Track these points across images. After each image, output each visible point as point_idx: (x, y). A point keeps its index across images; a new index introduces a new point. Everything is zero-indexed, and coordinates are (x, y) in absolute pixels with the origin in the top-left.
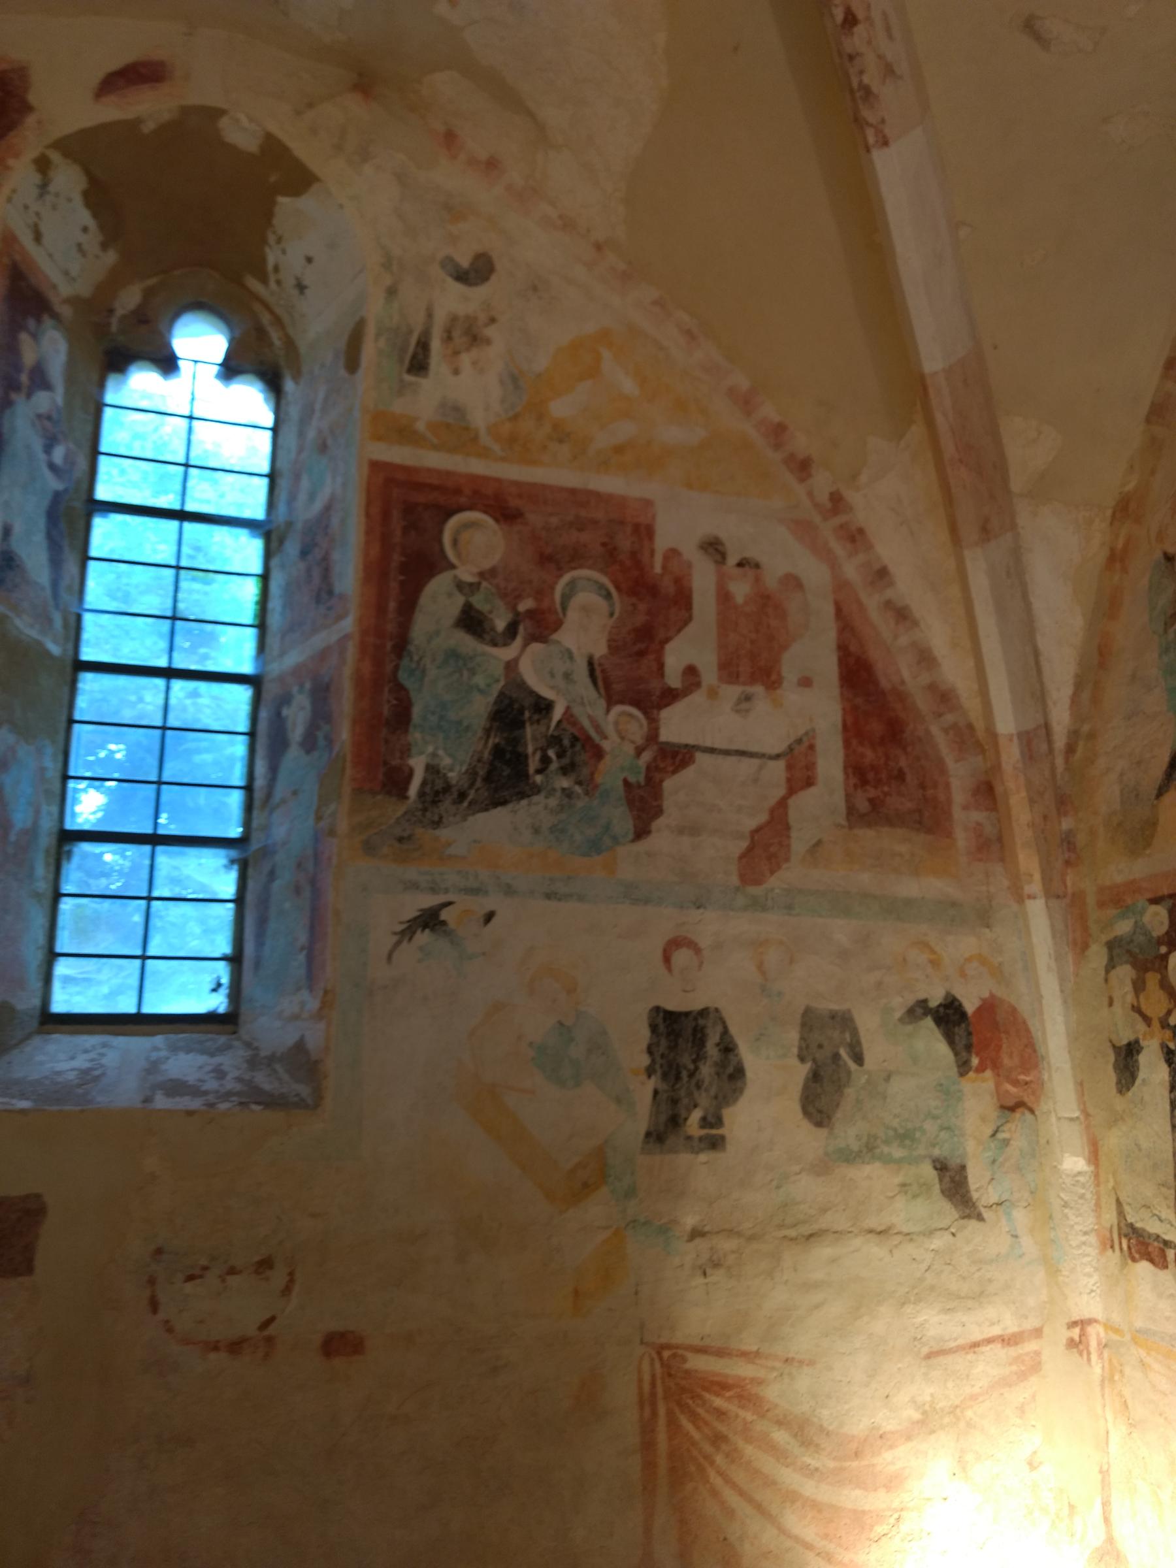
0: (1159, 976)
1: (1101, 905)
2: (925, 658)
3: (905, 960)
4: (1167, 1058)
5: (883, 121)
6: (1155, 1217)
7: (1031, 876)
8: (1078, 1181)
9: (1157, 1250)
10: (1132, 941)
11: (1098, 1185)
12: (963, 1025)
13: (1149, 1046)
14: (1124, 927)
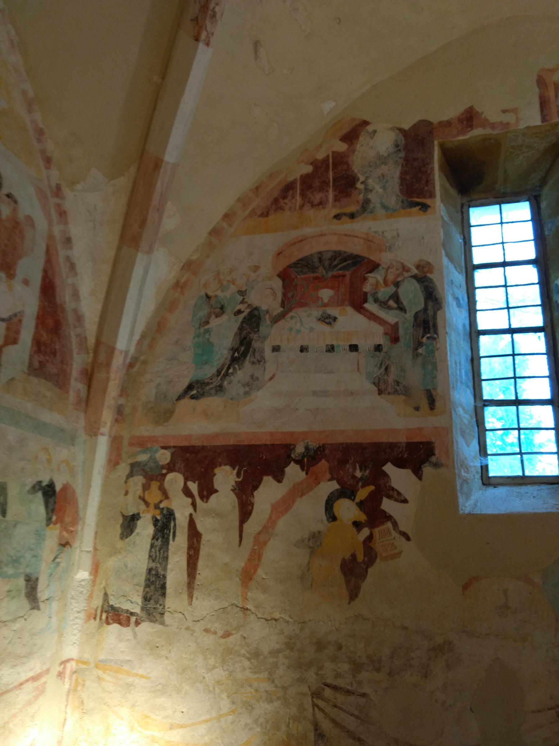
0: (159, 484)
1: (131, 444)
2: (76, 295)
3: (37, 457)
4: (155, 523)
5: (212, 34)
6: (129, 601)
7: (106, 423)
8: (81, 584)
9: (125, 617)
10: (146, 465)
11: (94, 586)
12: (53, 497)
13: (145, 517)
14: (143, 458)
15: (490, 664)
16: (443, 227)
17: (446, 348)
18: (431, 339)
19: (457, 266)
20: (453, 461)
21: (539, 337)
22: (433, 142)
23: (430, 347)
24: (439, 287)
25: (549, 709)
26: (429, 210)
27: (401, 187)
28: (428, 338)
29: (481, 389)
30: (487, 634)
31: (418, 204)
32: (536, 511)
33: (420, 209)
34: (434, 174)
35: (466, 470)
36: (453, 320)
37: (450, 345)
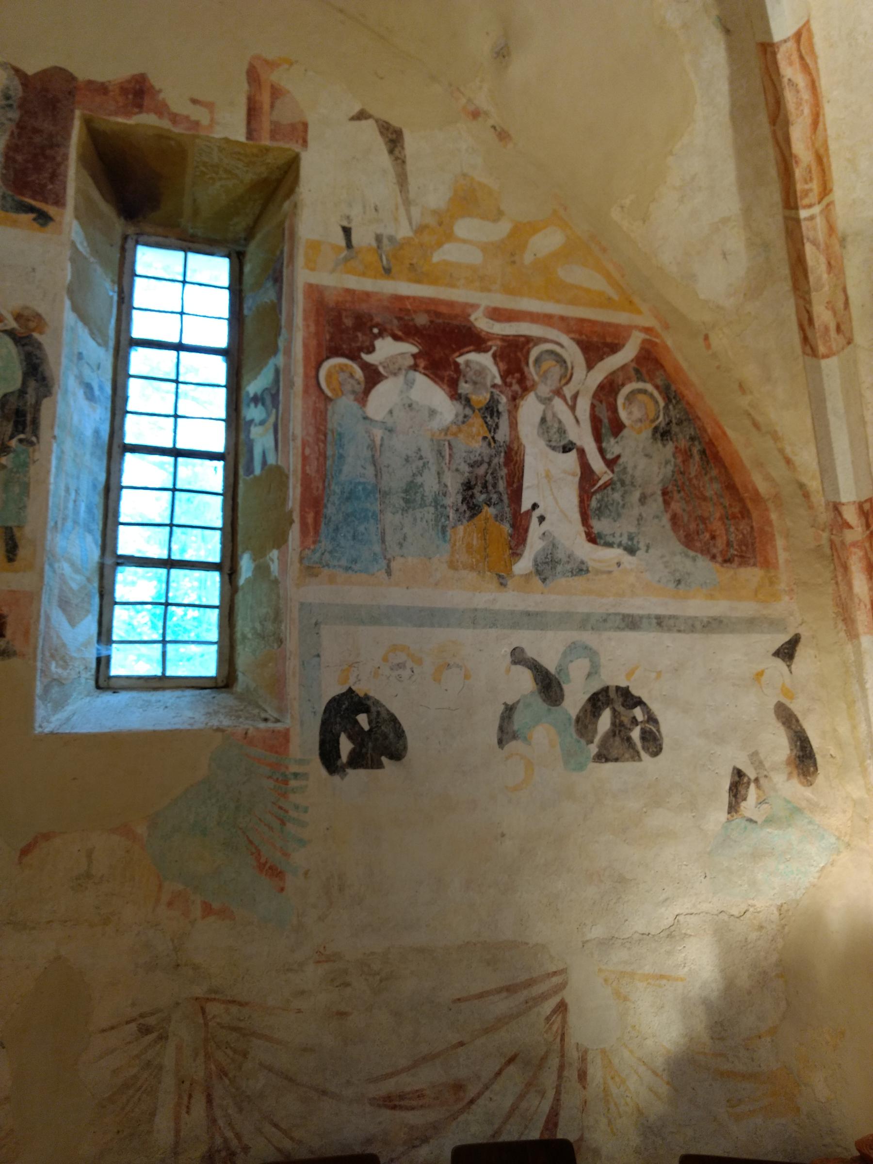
15: (46, 968)
16: (73, 260)
17: (49, 461)
18: (25, 443)
19: (95, 331)
20: (35, 648)
21: (216, 467)
22: (72, 111)
23: (22, 457)
24: (51, 359)
25: (127, 1023)
26: (51, 225)
27: (4, 171)
28: (21, 441)
29: (115, 539)
30: (49, 922)
31: (31, 209)
32: (158, 728)
33: (34, 219)
34: (67, 167)
35: (61, 663)
36: (72, 418)
37: (60, 459)
